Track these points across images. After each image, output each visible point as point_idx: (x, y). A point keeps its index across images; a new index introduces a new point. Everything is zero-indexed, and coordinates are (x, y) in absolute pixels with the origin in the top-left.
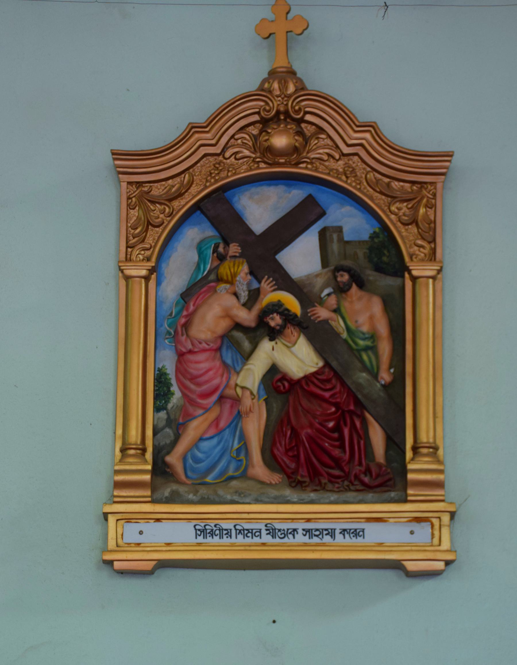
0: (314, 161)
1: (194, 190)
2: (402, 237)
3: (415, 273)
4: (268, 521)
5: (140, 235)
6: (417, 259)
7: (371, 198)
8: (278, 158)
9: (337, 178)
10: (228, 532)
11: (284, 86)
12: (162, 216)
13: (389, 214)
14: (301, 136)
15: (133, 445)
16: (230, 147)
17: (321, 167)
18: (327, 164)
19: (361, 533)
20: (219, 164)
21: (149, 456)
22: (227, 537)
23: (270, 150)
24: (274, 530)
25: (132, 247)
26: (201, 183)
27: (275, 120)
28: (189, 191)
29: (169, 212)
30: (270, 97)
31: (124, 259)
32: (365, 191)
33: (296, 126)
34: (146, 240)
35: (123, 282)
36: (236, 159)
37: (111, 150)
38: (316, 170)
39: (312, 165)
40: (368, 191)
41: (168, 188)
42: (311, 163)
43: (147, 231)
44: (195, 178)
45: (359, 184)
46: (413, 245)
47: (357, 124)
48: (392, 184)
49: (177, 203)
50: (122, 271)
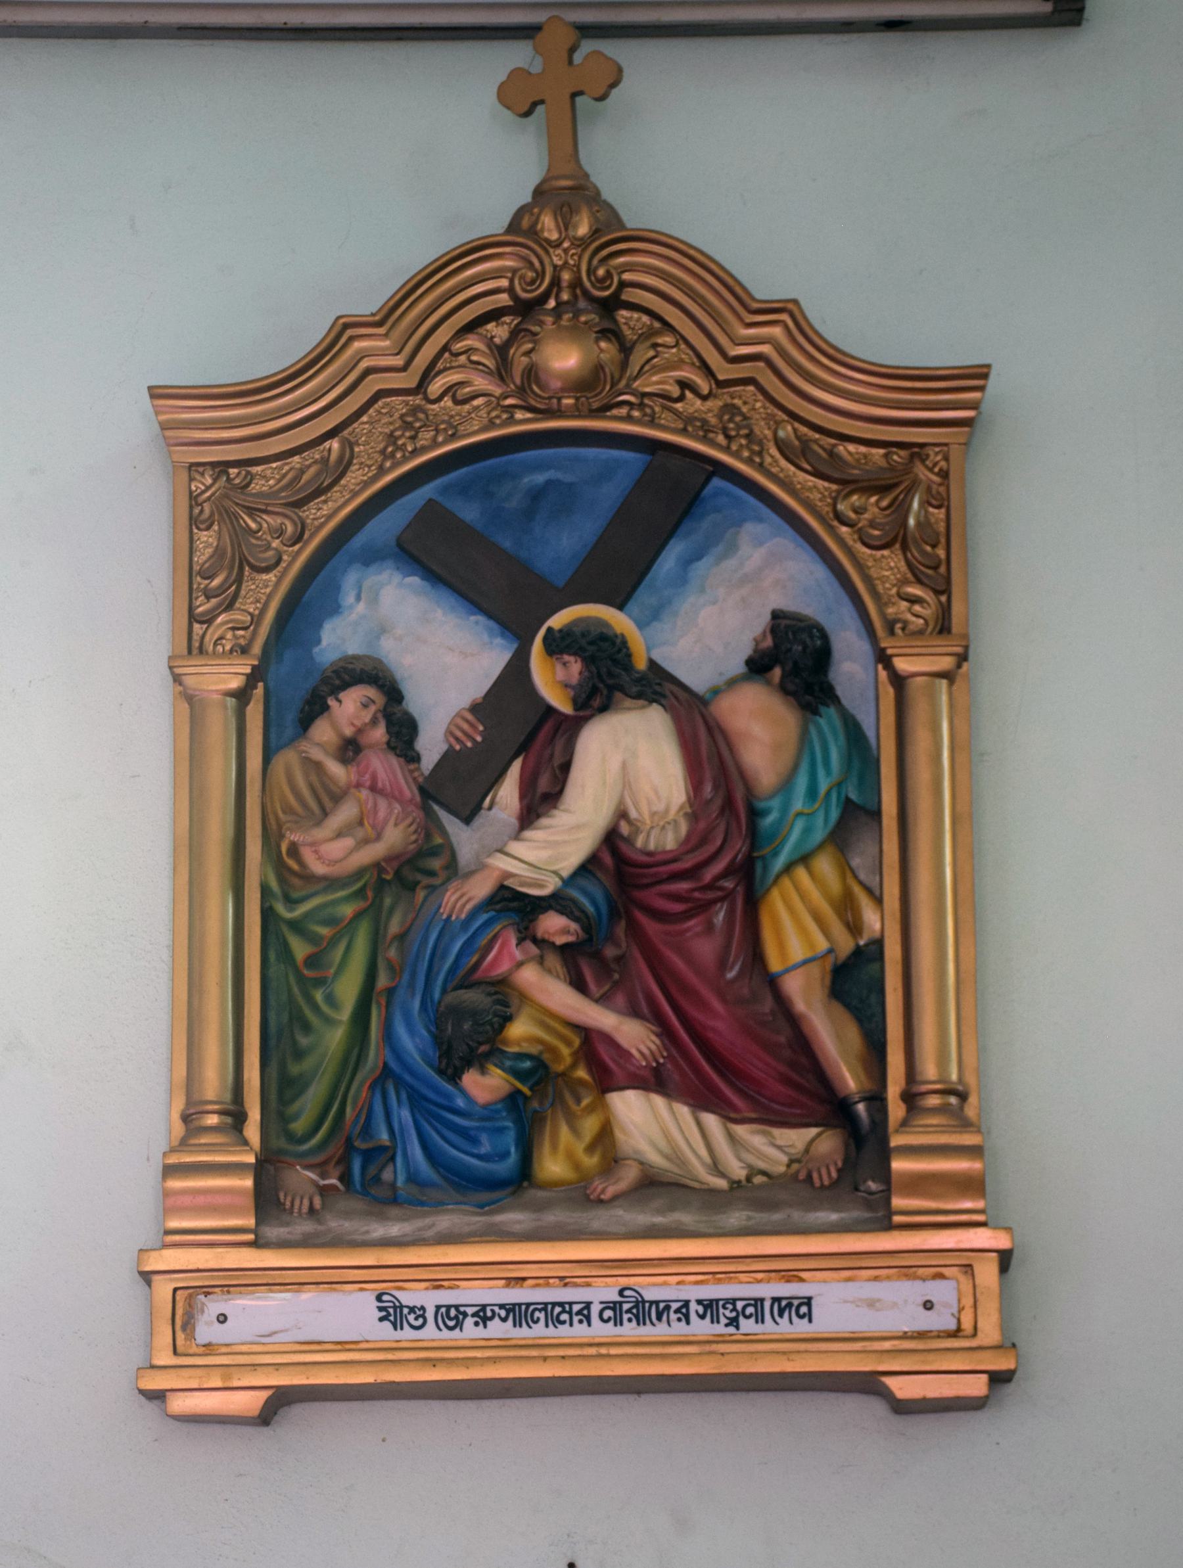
1: (355, 478)
3: (902, 665)
6: (907, 632)
9: (705, 439)
12: (276, 544)
13: (835, 523)
14: (613, 339)
18: (679, 406)
19: (804, 1309)
21: (252, 1132)
24: (398, 1310)
25: (208, 620)
26: (369, 462)
28: (343, 482)
29: (294, 533)
31: (185, 652)
32: (775, 470)
33: (601, 317)
34: (237, 605)
36: (457, 402)
37: (150, 388)
38: (652, 422)
42: (641, 406)
43: (239, 581)
44: (356, 449)
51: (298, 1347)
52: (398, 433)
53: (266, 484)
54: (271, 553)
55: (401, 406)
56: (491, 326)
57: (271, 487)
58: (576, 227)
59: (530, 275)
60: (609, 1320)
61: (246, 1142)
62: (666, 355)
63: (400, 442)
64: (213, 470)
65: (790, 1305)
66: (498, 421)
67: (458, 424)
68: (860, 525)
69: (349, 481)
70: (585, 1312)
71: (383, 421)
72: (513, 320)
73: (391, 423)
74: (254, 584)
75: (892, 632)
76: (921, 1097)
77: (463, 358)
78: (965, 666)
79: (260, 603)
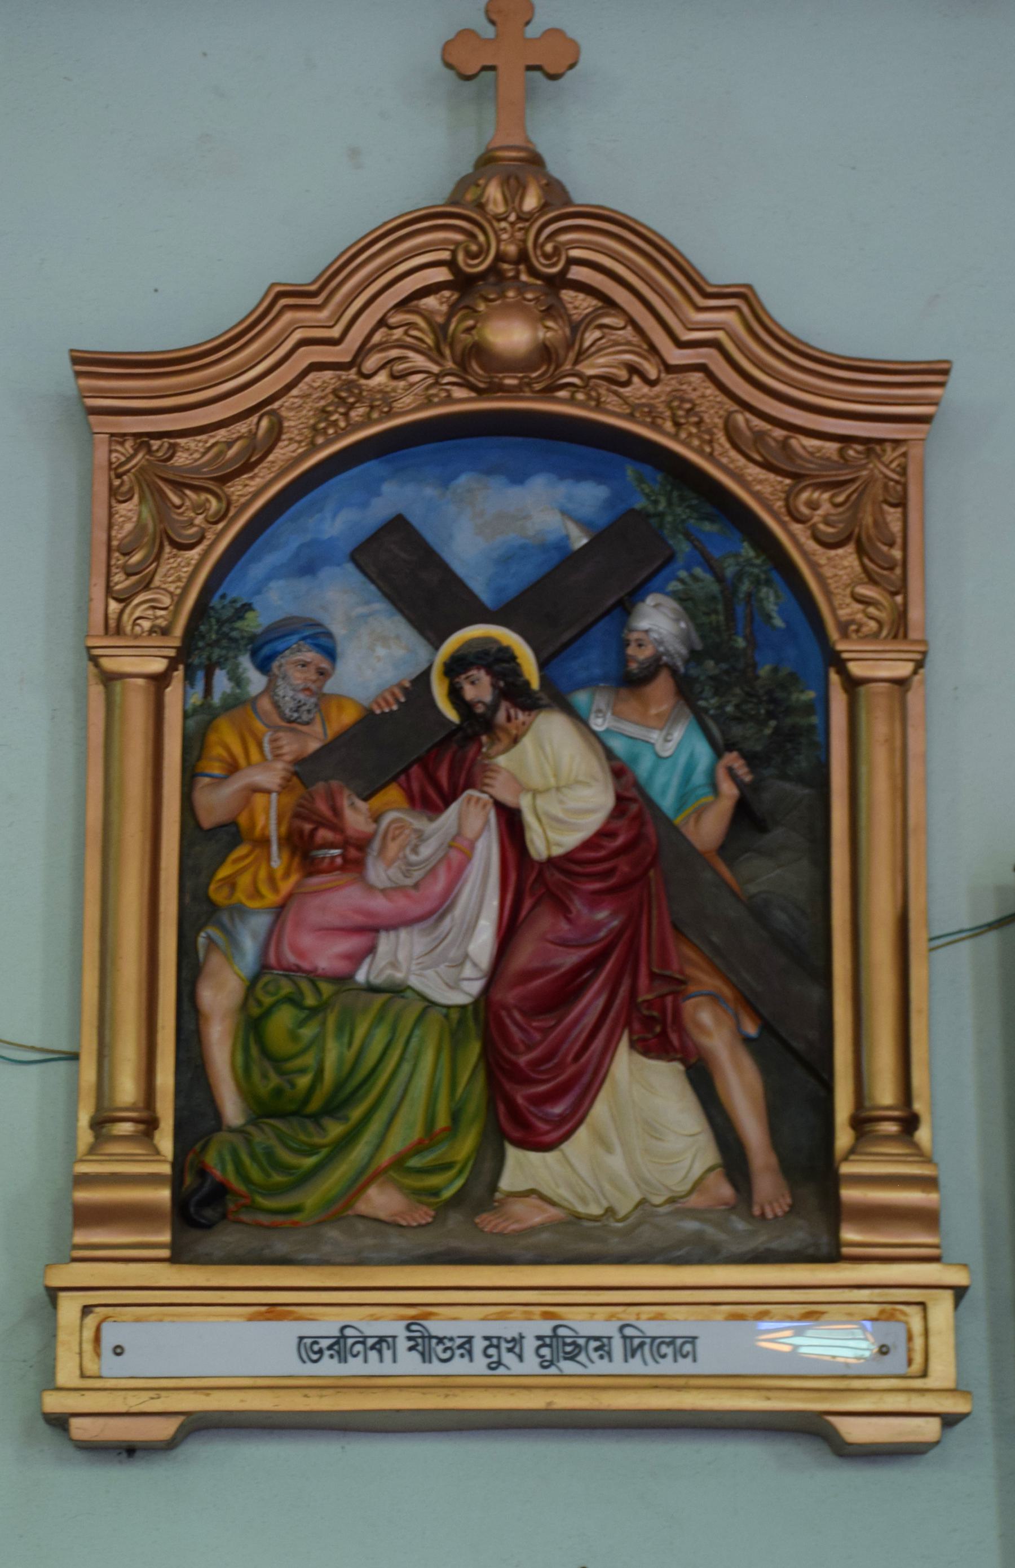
0: (593, 382)
3: (856, 669)
5: (144, 566)
8: (501, 375)
9: (654, 426)
10: (417, 1345)
11: (514, 188)
12: (199, 520)
13: (787, 519)
15: (127, 1109)
17: (613, 398)
21: (165, 1141)
22: (332, 1356)
23: (479, 351)
26: (298, 438)
27: (492, 279)
28: (271, 458)
29: (217, 512)
30: (479, 218)
32: (724, 460)
35: (97, 691)
36: (394, 377)
38: (599, 407)
40: (732, 461)
41: (215, 450)
43: (158, 558)
46: (849, 600)
47: (710, 290)
48: (793, 442)
49: (240, 487)
50: (94, 660)
53: (190, 458)
54: (194, 530)
57: (196, 460)
60: (489, 1356)
61: (157, 1152)
62: (613, 337)
64: (135, 440)
65: (641, 1345)
66: (436, 400)
70: (467, 1346)
71: (314, 396)
73: (322, 398)
75: (845, 635)
78: (921, 671)
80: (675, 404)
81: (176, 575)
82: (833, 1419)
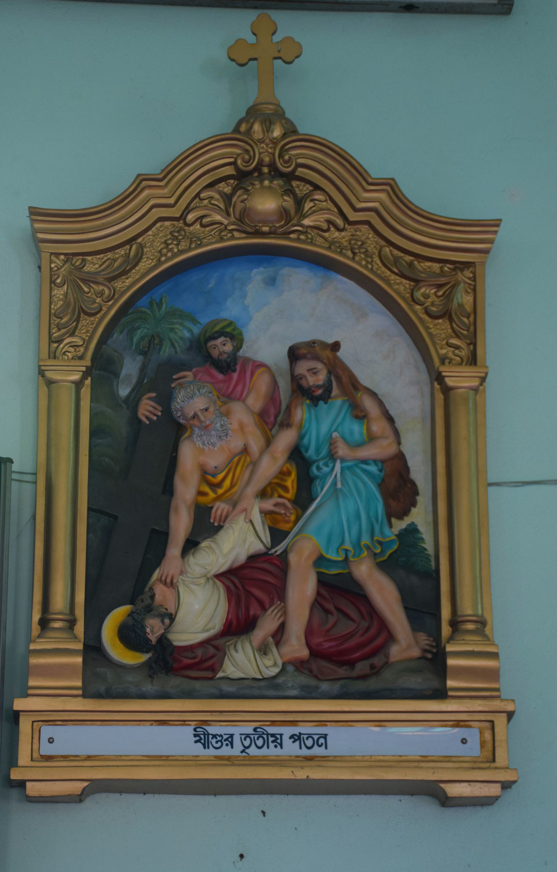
2: (431, 335)
3: (450, 382)
4: (257, 724)
5: (68, 325)
7: (386, 281)
9: (341, 253)
12: (98, 300)
15: (59, 613)
16: (193, 209)
18: (326, 235)
19: (322, 741)
20: (178, 232)
21: (80, 628)
24: (206, 736)
26: (152, 257)
27: (256, 174)
28: (137, 268)
29: (109, 296)
31: (47, 358)
32: (379, 272)
34: (76, 334)
36: (202, 226)
37: (30, 208)
39: (306, 236)
43: (78, 320)
44: (145, 250)
45: (371, 263)
47: (370, 180)
49: (120, 283)
51: (143, 758)
52: (170, 242)
53: (93, 267)
54: (96, 305)
55: (171, 227)
56: (222, 185)
57: (96, 269)
58: (273, 132)
59: (247, 157)
61: (75, 637)
62: (320, 206)
63: (170, 247)
66: (225, 238)
67: (203, 238)
68: (426, 305)
69: (141, 267)
72: (234, 182)
74: (85, 322)
76: (462, 624)
77: (206, 202)
79: (89, 333)
80: (353, 242)
81: (86, 329)
82: (442, 785)
